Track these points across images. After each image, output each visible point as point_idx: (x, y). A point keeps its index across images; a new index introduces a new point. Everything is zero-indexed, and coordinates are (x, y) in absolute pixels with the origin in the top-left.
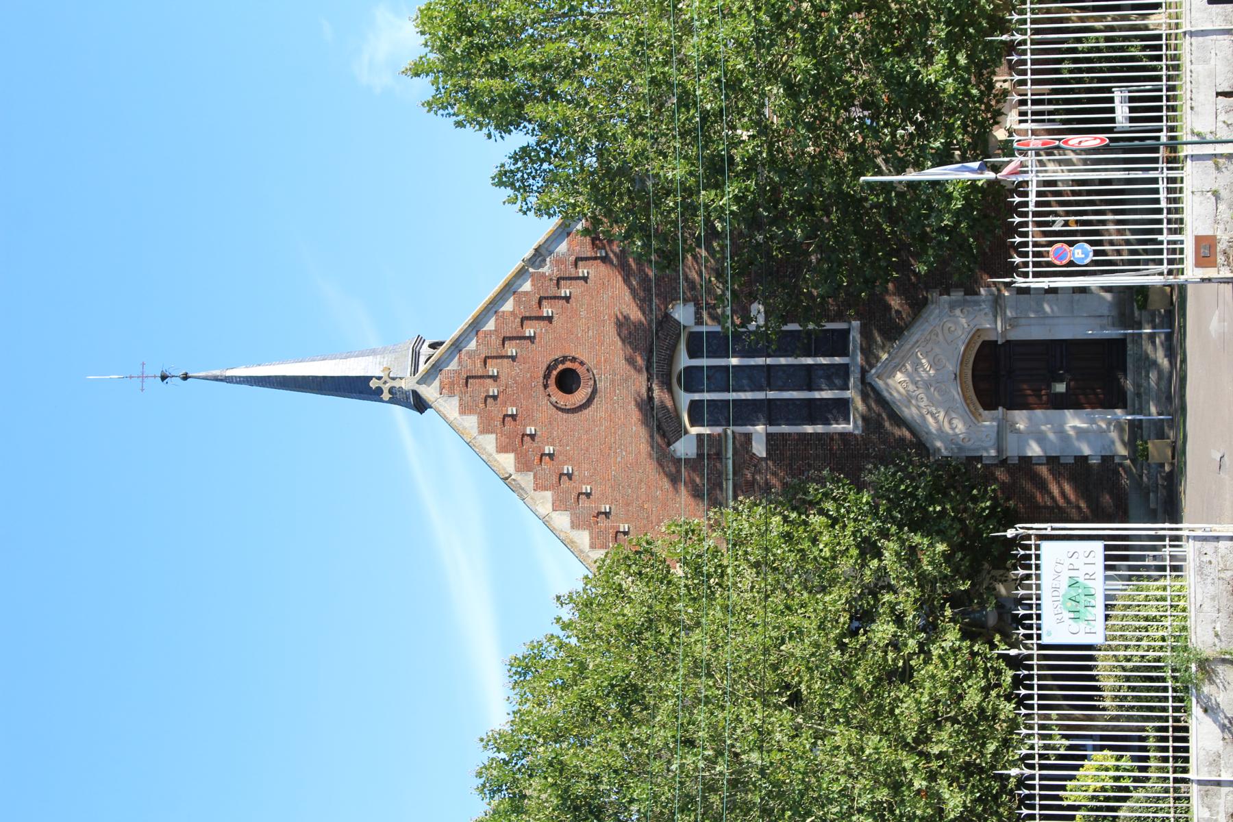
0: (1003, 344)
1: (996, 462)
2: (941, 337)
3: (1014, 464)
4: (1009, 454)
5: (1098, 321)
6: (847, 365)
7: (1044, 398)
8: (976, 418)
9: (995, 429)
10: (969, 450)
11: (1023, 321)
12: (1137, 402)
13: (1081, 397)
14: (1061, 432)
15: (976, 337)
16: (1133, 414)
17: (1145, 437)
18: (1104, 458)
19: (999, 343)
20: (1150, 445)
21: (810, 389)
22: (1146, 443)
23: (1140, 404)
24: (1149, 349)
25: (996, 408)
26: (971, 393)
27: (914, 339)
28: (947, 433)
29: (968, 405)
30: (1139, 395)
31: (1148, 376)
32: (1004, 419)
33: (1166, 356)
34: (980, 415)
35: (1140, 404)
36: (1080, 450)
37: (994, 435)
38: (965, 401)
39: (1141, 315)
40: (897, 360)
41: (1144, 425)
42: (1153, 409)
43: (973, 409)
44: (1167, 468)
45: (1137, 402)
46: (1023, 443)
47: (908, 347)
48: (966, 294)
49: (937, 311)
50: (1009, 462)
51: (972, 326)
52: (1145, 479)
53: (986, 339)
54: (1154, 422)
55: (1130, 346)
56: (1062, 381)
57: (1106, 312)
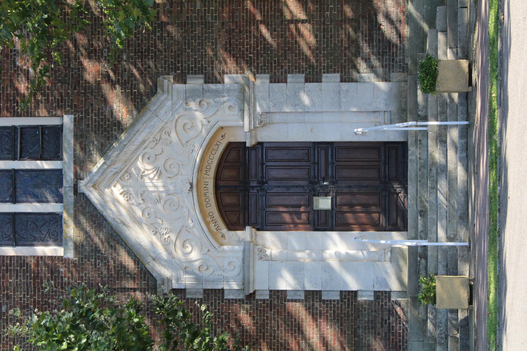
0: (254, 147)
1: (241, 297)
2: (173, 135)
3: (264, 300)
4: (257, 288)
5: (372, 118)
6: (60, 171)
7: (304, 216)
8: (216, 240)
9: (240, 255)
10: (207, 281)
11: (277, 118)
12: (420, 222)
13: (349, 215)
14: (229, 338)
15: (219, 138)
16: (416, 238)
17: (431, 270)
18: (378, 295)
19: (248, 145)
20: (437, 284)
21: (15, 200)
22: (432, 280)
23: (425, 225)
24: (437, 155)
25: (243, 228)
26: (213, 208)
27: (140, 138)
28: (179, 260)
29: (207, 224)
30: (423, 213)
31: (435, 189)
32: (254, 242)
33: (461, 159)
34: (223, 236)
35: (425, 225)
36: (345, 283)
37: (238, 263)
38: (204, 219)
39: (426, 100)
40: (118, 165)
41: (429, 254)
42: (441, 233)
43: (214, 229)
44: (461, 316)
45: (420, 222)
46: (275, 274)
47: (133, 148)
48: (206, 82)
49: (169, 103)
50: (257, 297)
51: (212, 123)
52: (430, 326)
53: (232, 140)
54: (446, 250)
55: (411, 149)
56: (326, 195)
57: (382, 107)
